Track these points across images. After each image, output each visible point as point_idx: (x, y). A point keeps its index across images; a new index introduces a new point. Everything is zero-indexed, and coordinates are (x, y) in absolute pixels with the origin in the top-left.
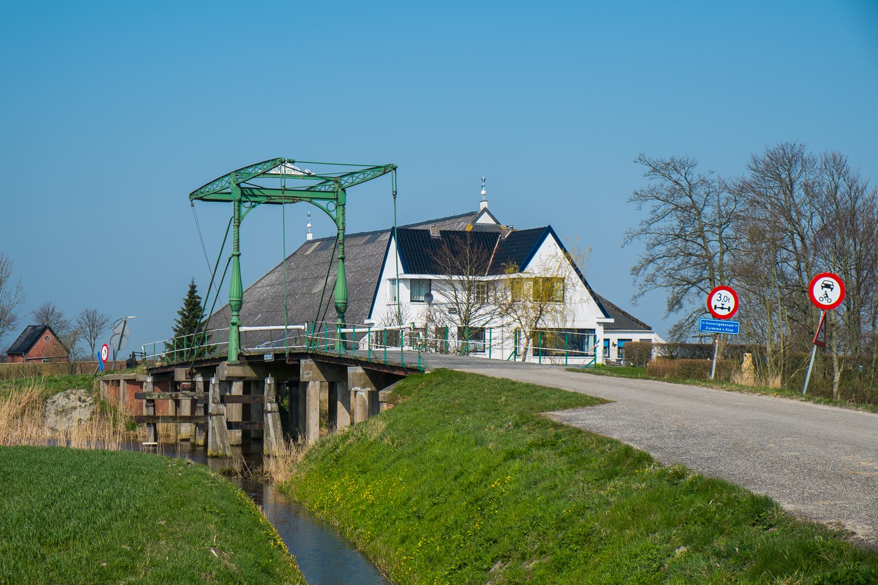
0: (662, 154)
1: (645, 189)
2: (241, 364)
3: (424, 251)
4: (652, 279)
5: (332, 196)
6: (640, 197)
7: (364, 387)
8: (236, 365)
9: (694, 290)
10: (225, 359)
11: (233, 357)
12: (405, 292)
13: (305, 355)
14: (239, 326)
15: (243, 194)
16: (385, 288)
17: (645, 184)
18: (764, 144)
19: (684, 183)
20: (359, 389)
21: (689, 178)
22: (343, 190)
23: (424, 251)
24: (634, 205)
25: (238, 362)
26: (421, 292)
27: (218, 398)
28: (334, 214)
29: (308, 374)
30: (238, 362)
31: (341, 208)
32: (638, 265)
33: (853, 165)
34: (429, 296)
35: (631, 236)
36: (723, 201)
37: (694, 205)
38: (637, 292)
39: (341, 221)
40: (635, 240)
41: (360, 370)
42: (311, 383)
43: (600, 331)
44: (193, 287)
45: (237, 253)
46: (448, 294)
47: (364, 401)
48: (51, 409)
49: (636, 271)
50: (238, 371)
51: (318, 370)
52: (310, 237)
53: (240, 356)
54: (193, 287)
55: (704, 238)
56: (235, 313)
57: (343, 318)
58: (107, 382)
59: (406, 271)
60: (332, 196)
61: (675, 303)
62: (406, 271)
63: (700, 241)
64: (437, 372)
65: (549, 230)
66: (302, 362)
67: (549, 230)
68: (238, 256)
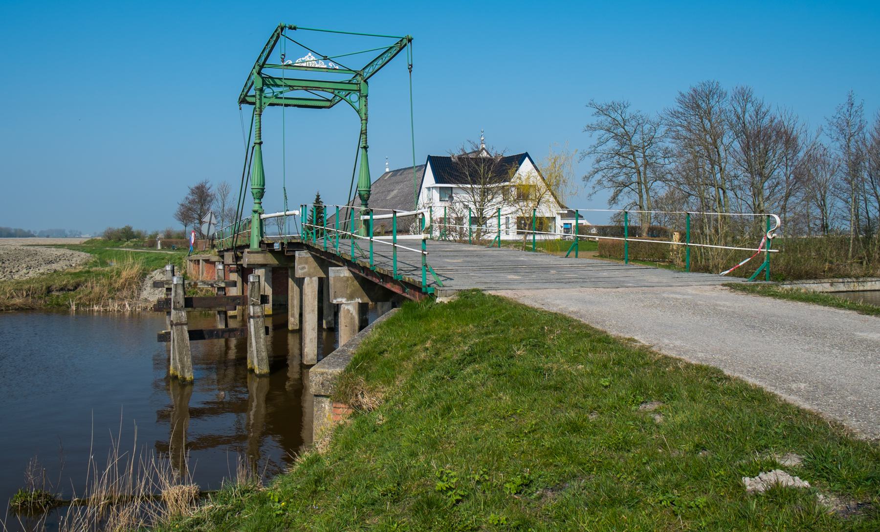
0: (603, 100)
1: (595, 123)
2: (262, 252)
3: (447, 170)
4: (600, 182)
5: (355, 87)
6: (591, 128)
7: (351, 297)
8: (257, 252)
9: (626, 189)
10: (248, 246)
11: (255, 245)
12: (436, 195)
13: (300, 246)
14: (260, 214)
15: (264, 84)
16: (424, 193)
17: (595, 120)
18: (688, 82)
19: (619, 118)
20: (344, 300)
21: (623, 115)
22: (365, 81)
23: (447, 170)
24: (588, 133)
25: (260, 249)
26: (446, 194)
27: (182, 302)
28: (356, 105)
29: (303, 268)
30: (260, 249)
31: (364, 99)
32: (587, 175)
33: (757, 95)
34: (451, 197)
35: (584, 156)
36: (646, 131)
37: (627, 133)
38: (591, 191)
39: (363, 111)
40: (587, 158)
41: (344, 272)
42: (307, 280)
43: (558, 218)
44: (318, 196)
45: (258, 141)
46: (465, 198)
47: (352, 318)
48: (149, 283)
49: (586, 178)
50: (259, 259)
51: (315, 264)
52: (387, 170)
53: (261, 243)
54: (318, 196)
55: (634, 156)
56: (257, 201)
57: (366, 205)
58: (191, 261)
59: (437, 182)
60: (355, 87)
61: (614, 199)
62: (437, 182)
63: (631, 157)
64: (470, 303)
65: (526, 155)
66: (297, 253)
67: (526, 155)
68: (260, 143)
